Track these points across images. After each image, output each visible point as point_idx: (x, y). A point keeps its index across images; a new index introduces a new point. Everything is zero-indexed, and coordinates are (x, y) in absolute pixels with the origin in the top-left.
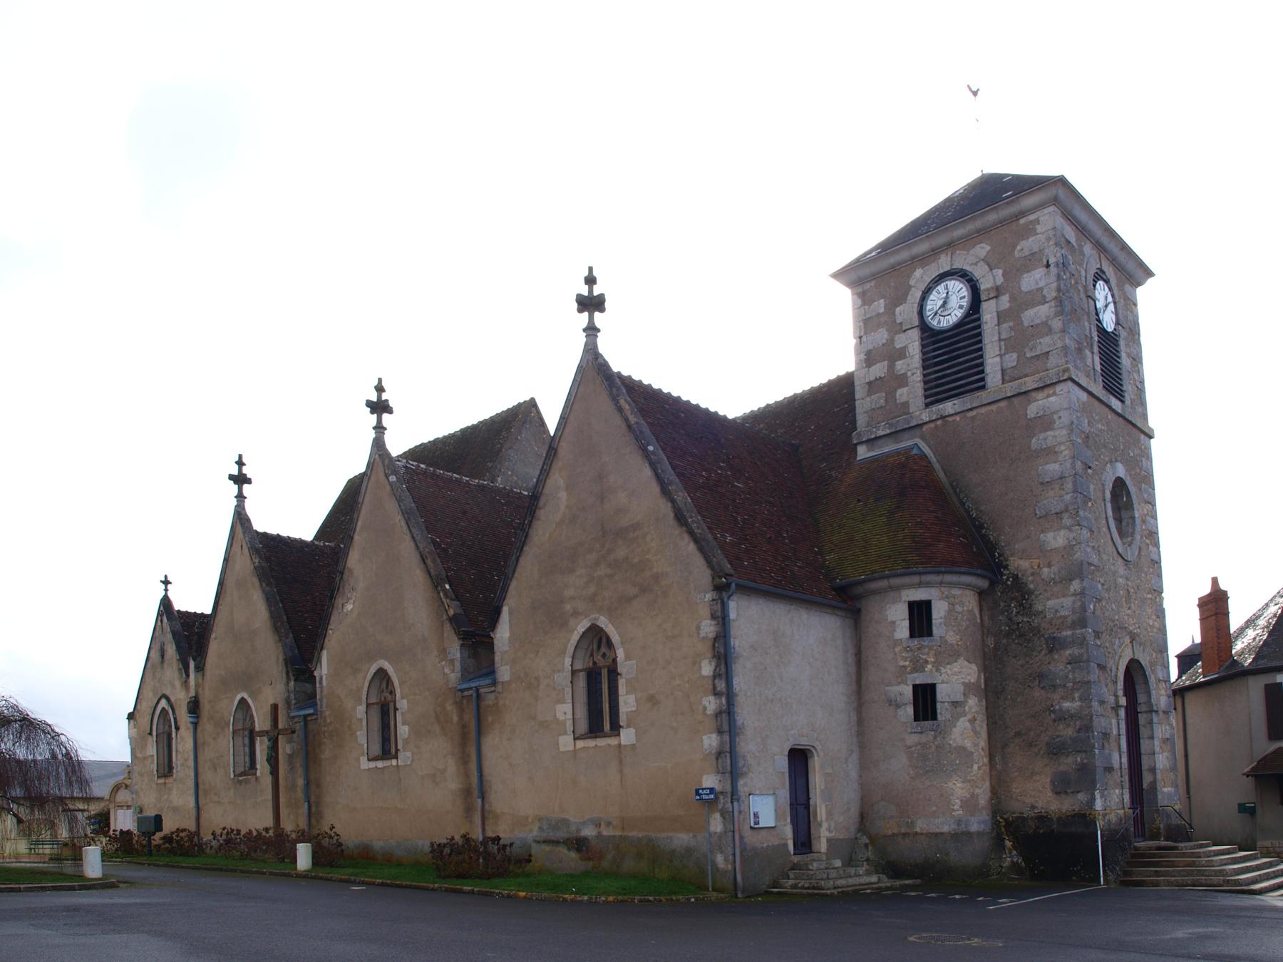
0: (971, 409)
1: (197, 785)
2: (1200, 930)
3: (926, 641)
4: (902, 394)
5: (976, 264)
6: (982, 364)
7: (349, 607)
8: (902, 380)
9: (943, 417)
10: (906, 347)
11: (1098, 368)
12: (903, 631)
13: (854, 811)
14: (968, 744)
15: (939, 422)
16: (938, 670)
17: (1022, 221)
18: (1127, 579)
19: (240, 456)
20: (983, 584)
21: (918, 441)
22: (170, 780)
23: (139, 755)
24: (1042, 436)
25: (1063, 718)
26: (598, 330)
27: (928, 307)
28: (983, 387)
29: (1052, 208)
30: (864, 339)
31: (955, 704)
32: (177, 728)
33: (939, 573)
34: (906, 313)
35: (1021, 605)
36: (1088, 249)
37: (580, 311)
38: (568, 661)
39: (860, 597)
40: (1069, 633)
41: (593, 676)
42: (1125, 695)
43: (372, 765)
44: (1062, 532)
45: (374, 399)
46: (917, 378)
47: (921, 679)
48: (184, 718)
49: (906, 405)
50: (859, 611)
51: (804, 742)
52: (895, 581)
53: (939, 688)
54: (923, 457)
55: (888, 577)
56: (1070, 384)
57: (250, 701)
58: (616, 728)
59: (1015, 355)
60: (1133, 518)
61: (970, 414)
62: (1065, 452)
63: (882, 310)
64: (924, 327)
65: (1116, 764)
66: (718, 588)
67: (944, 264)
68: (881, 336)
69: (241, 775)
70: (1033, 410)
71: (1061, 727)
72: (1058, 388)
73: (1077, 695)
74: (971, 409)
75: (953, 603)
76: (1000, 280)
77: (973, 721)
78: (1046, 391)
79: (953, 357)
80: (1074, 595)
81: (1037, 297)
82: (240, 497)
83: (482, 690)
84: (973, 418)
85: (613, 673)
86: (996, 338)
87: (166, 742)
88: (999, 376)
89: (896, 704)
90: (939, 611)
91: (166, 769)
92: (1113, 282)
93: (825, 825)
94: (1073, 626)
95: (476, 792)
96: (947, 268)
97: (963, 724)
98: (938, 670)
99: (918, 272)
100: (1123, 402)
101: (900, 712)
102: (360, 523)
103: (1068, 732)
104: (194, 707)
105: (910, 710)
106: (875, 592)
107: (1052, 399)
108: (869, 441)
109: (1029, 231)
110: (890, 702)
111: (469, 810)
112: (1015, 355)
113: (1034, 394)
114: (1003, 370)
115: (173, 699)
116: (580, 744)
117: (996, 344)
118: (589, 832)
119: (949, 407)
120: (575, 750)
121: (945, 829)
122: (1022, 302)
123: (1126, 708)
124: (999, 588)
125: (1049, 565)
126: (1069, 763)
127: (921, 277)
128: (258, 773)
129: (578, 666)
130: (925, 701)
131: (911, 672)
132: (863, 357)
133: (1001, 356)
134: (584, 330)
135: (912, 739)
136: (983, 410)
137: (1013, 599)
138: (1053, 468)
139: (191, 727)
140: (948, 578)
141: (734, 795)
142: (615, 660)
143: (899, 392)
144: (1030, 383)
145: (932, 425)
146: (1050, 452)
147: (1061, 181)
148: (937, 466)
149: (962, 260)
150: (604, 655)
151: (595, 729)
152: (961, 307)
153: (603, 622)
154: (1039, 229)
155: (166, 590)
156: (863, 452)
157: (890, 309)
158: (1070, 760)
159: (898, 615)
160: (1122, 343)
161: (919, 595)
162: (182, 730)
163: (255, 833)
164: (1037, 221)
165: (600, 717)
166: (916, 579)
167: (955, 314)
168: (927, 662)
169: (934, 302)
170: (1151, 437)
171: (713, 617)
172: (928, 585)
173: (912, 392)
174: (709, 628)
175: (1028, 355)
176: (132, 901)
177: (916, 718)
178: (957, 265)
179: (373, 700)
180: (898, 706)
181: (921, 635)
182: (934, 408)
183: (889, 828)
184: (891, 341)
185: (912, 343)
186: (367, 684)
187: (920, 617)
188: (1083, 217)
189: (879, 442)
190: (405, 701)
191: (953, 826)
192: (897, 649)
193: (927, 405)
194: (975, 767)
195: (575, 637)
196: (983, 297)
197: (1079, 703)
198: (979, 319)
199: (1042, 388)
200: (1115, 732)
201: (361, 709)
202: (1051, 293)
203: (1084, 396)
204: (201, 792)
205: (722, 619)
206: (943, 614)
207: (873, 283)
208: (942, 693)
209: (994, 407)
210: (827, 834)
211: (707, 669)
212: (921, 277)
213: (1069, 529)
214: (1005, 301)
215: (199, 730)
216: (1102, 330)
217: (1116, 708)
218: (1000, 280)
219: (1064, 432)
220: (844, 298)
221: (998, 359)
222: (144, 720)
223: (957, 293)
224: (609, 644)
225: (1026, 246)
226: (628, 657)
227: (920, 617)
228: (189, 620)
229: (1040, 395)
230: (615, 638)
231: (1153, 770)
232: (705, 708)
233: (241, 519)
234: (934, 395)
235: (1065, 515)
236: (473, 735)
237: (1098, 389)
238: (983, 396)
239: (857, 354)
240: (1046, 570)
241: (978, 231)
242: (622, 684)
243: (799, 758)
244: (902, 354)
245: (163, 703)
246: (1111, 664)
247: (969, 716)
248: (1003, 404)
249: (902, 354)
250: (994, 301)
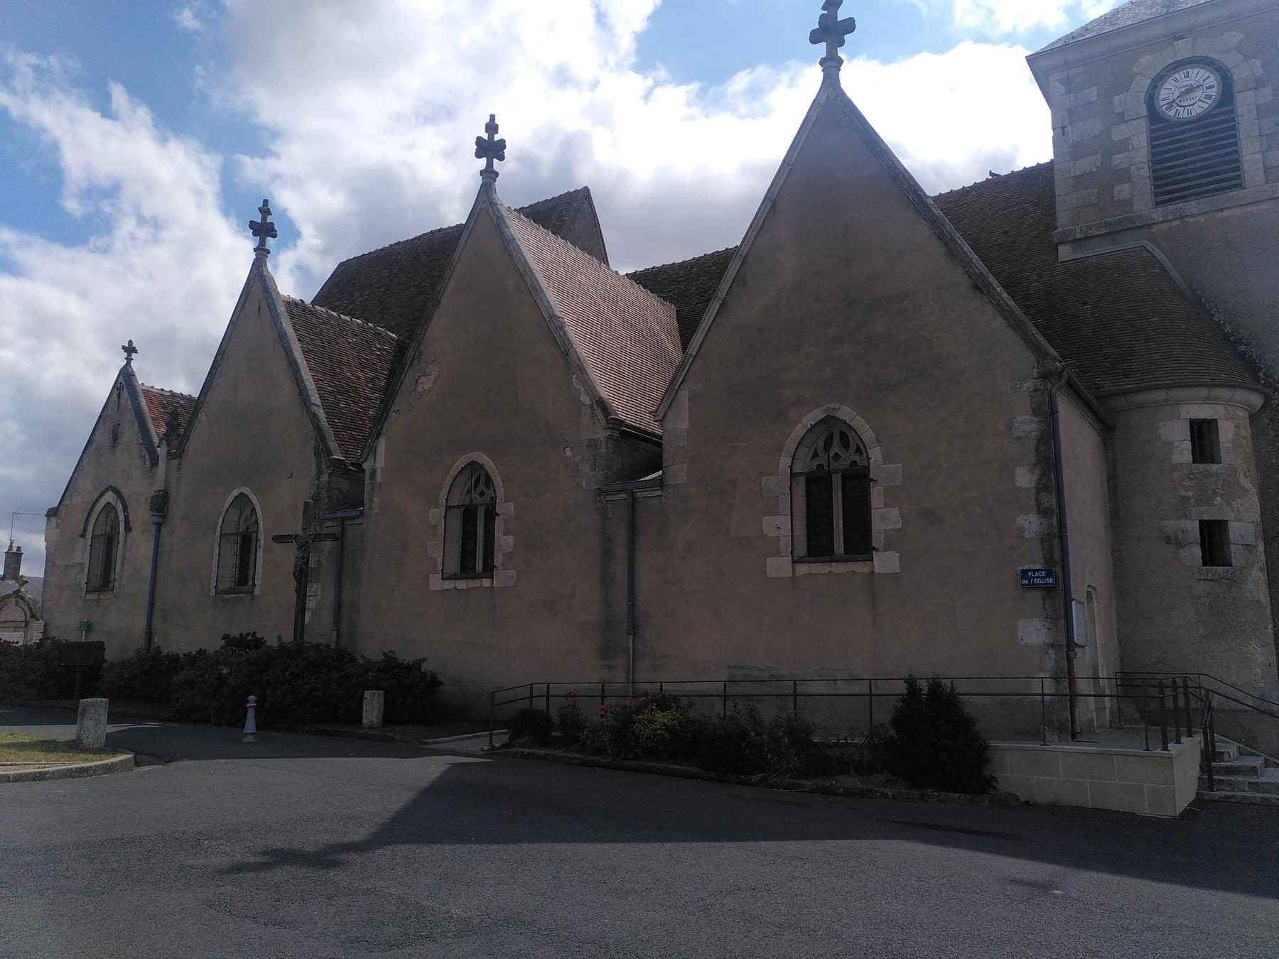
1: (152, 604)
2: (689, 769)
5: (1226, 52)
7: (426, 384)
9: (1182, 218)
12: (1183, 453)
16: (1229, 505)
22: (108, 596)
23: (59, 562)
27: (1162, 97)
28: (1239, 186)
30: (1068, 129)
32: (128, 529)
37: (478, 155)
38: (785, 462)
41: (469, 516)
43: (449, 585)
45: (485, 136)
48: (141, 514)
49: (1128, 203)
52: (1176, 393)
55: (1168, 387)
57: (253, 498)
58: (489, 570)
63: (1094, 99)
64: (1154, 116)
68: (1094, 126)
69: (227, 591)
76: (1259, 71)
83: (639, 495)
85: (491, 515)
86: (1257, 133)
87: (107, 545)
89: (1175, 542)
90: (1226, 432)
91: (103, 581)
95: (624, 627)
98: (1229, 505)
99: (1146, 59)
102: (451, 285)
104: (161, 504)
105: (1197, 551)
110: (1168, 540)
111: (606, 652)
115: (125, 493)
116: (803, 569)
120: (794, 579)
128: (257, 591)
129: (454, 502)
130: (1213, 539)
132: (1066, 149)
139: (153, 528)
142: (493, 499)
143: (1117, 189)
150: (482, 494)
151: (467, 570)
152: (1209, 97)
153: (846, 413)
155: (129, 360)
156: (1065, 252)
159: (1177, 437)
161: (1203, 412)
162: (136, 533)
163: (924, 687)
165: (474, 556)
167: (1197, 106)
169: (1169, 90)
171: (1035, 412)
172: (1214, 401)
176: (114, 760)
178: (1200, 52)
179: (231, 528)
180: (1180, 545)
186: (448, 481)
187: (1203, 434)
190: (511, 505)
193: (1158, 204)
195: (799, 431)
198: (1232, 111)
201: (437, 514)
204: (157, 613)
206: (1230, 437)
207: (1082, 69)
211: (1025, 478)
215: (164, 531)
218: (1259, 71)
221: (1259, 156)
222: (77, 519)
224: (489, 481)
226: (888, 458)
227: (1203, 434)
230: (498, 480)
232: (1022, 530)
236: (621, 552)
242: (499, 524)
245: (109, 497)
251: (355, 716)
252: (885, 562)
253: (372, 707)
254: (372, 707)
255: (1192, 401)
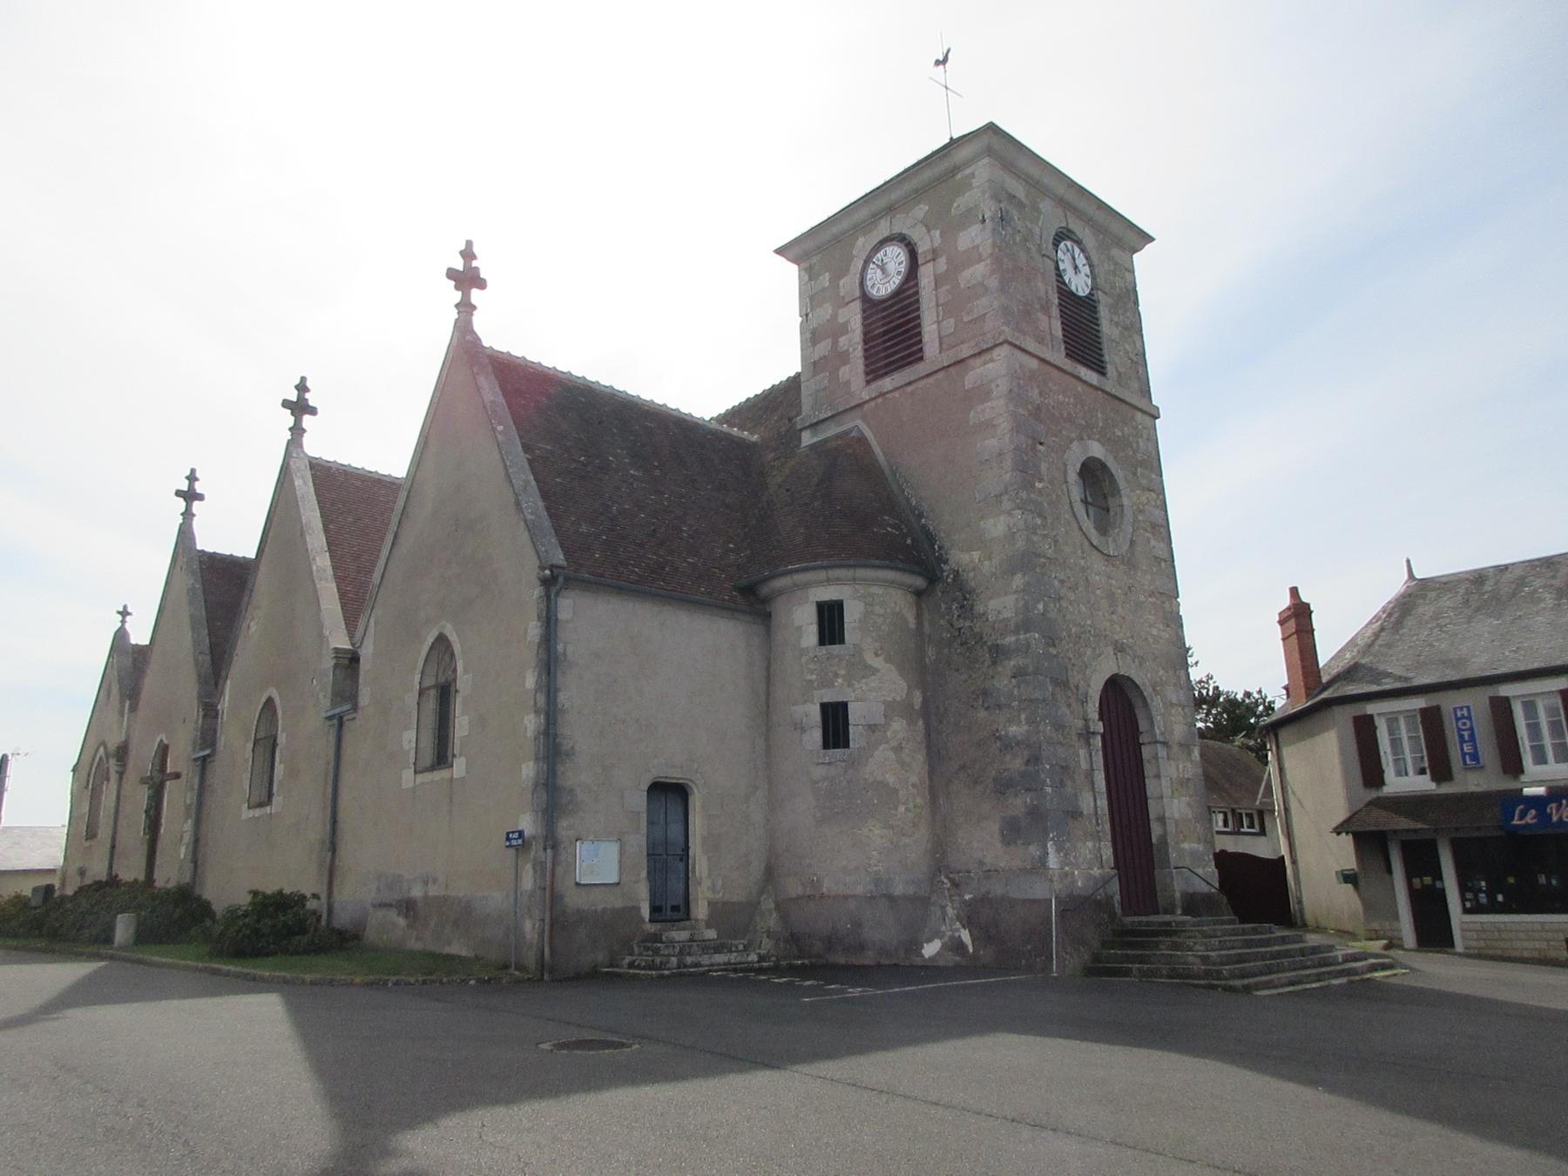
0: (910, 383)
1: (113, 847)
3: (836, 649)
4: (844, 373)
6: (919, 333)
8: (843, 358)
9: (882, 395)
10: (848, 321)
11: (1059, 333)
12: (810, 636)
13: (757, 869)
14: (891, 779)
15: (880, 400)
17: (959, 176)
18: (1109, 577)
19: (193, 471)
20: (920, 582)
21: (859, 422)
24: (979, 408)
25: (1008, 745)
26: (474, 308)
28: (921, 358)
29: (986, 160)
31: (872, 728)
33: (849, 567)
34: (849, 285)
35: (962, 607)
36: (1046, 206)
38: (417, 677)
39: (766, 600)
40: (1013, 639)
42: (1101, 718)
43: (251, 813)
44: (1002, 518)
46: (858, 353)
47: (830, 696)
49: (848, 383)
50: (769, 615)
51: (674, 775)
53: (851, 707)
54: (862, 440)
56: (1006, 346)
59: (952, 321)
60: (1122, 506)
61: (909, 389)
62: (1004, 425)
64: (865, 298)
65: (1086, 803)
66: (547, 583)
67: (884, 229)
68: (825, 312)
70: (970, 379)
71: (1008, 757)
72: (996, 352)
73: (1023, 717)
74: (910, 383)
75: (873, 600)
76: (937, 241)
77: (898, 749)
78: (986, 357)
79: (893, 332)
80: (1016, 592)
81: (972, 256)
82: (188, 515)
84: (912, 393)
88: (937, 344)
90: (852, 614)
92: (1090, 242)
93: (706, 883)
94: (1016, 632)
96: (886, 234)
97: (883, 753)
99: (861, 240)
100: (1101, 371)
101: (806, 737)
103: (1016, 764)
105: (817, 735)
106: (780, 592)
107: (990, 365)
108: (813, 426)
109: (966, 186)
112: (952, 321)
113: (971, 362)
114: (941, 339)
116: (421, 778)
117: (934, 311)
118: (417, 892)
119: (887, 383)
121: (859, 890)
122: (957, 266)
123: (1103, 736)
124: (939, 587)
125: (990, 559)
126: (1018, 804)
127: (863, 244)
131: (818, 688)
132: (808, 335)
133: (938, 322)
134: (457, 306)
135: (818, 772)
136: (921, 384)
137: (954, 600)
138: (992, 443)
140: (861, 573)
141: (551, 841)
144: (965, 351)
145: (873, 404)
146: (989, 425)
147: (991, 128)
148: (877, 450)
149: (901, 225)
154: (975, 182)
155: (123, 622)
156: (807, 439)
157: (835, 280)
158: (1018, 802)
159: (802, 620)
160: (1103, 312)
161: (828, 594)
164: (973, 175)
166: (822, 575)
168: (836, 675)
169: (873, 274)
170: (1156, 417)
173: (853, 372)
174: (534, 630)
175: (966, 319)
177: (826, 746)
178: (896, 230)
180: (803, 730)
181: (832, 642)
182: (874, 386)
183: (793, 888)
184: (834, 316)
185: (853, 317)
187: (831, 622)
188: (1033, 170)
189: (823, 426)
191: (872, 887)
192: (804, 660)
194: (902, 809)
196: (920, 261)
197: (1026, 727)
199: (980, 353)
200: (1084, 765)
202: (986, 249)
203: (1034, 364)
205: (550, 622)
206: (857, 616)
208: (855, 713)
209: (931, 380)
210: (710, 895)
212: (863, 244)
213: (1009, 513)
214: (942, 264)
216: (1065, 294)
217: (1086, 735)
219: (1002, 401)
220: (790, 273)
223: (895, 258)
225: (962, 202)
226: (466, 671)
227: (831, 622)
228: (140, 651)
229: (978, 361)
230: (457, 648)
231: (1162, 820)
233: (185, 534)
234: (874, 372)
235: (1005, 498)
237: (1059, 356)
238: (920, 369)
239: (802, 333)
240: (987, 563)
241: (916, 191)
243: (669, 794)
244: (844, 329)
246: (1075, 678)
247: (894, 744)
248: (940, 375)
249: (844, 329)
250: (930, 265)
251: (108, 940)
252: (459, 767)
253: (123, 928)
254: (123, 928)
255: (819, 583)
